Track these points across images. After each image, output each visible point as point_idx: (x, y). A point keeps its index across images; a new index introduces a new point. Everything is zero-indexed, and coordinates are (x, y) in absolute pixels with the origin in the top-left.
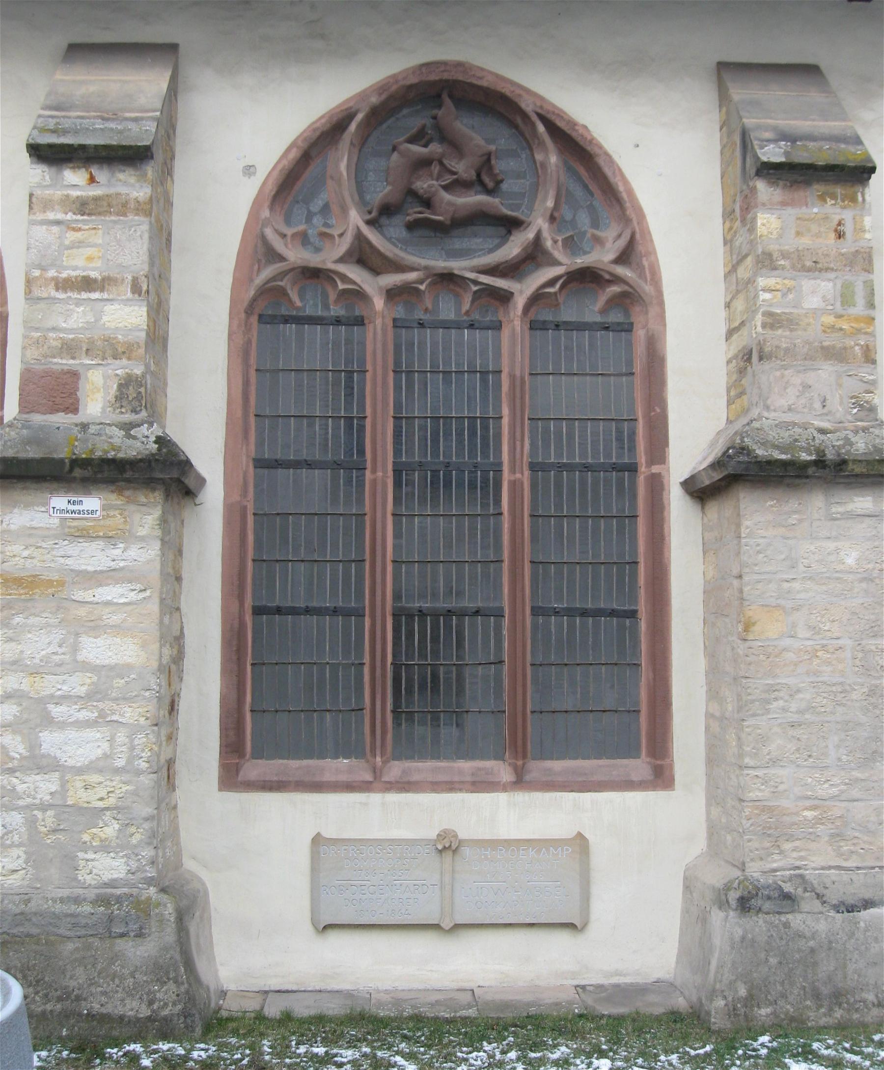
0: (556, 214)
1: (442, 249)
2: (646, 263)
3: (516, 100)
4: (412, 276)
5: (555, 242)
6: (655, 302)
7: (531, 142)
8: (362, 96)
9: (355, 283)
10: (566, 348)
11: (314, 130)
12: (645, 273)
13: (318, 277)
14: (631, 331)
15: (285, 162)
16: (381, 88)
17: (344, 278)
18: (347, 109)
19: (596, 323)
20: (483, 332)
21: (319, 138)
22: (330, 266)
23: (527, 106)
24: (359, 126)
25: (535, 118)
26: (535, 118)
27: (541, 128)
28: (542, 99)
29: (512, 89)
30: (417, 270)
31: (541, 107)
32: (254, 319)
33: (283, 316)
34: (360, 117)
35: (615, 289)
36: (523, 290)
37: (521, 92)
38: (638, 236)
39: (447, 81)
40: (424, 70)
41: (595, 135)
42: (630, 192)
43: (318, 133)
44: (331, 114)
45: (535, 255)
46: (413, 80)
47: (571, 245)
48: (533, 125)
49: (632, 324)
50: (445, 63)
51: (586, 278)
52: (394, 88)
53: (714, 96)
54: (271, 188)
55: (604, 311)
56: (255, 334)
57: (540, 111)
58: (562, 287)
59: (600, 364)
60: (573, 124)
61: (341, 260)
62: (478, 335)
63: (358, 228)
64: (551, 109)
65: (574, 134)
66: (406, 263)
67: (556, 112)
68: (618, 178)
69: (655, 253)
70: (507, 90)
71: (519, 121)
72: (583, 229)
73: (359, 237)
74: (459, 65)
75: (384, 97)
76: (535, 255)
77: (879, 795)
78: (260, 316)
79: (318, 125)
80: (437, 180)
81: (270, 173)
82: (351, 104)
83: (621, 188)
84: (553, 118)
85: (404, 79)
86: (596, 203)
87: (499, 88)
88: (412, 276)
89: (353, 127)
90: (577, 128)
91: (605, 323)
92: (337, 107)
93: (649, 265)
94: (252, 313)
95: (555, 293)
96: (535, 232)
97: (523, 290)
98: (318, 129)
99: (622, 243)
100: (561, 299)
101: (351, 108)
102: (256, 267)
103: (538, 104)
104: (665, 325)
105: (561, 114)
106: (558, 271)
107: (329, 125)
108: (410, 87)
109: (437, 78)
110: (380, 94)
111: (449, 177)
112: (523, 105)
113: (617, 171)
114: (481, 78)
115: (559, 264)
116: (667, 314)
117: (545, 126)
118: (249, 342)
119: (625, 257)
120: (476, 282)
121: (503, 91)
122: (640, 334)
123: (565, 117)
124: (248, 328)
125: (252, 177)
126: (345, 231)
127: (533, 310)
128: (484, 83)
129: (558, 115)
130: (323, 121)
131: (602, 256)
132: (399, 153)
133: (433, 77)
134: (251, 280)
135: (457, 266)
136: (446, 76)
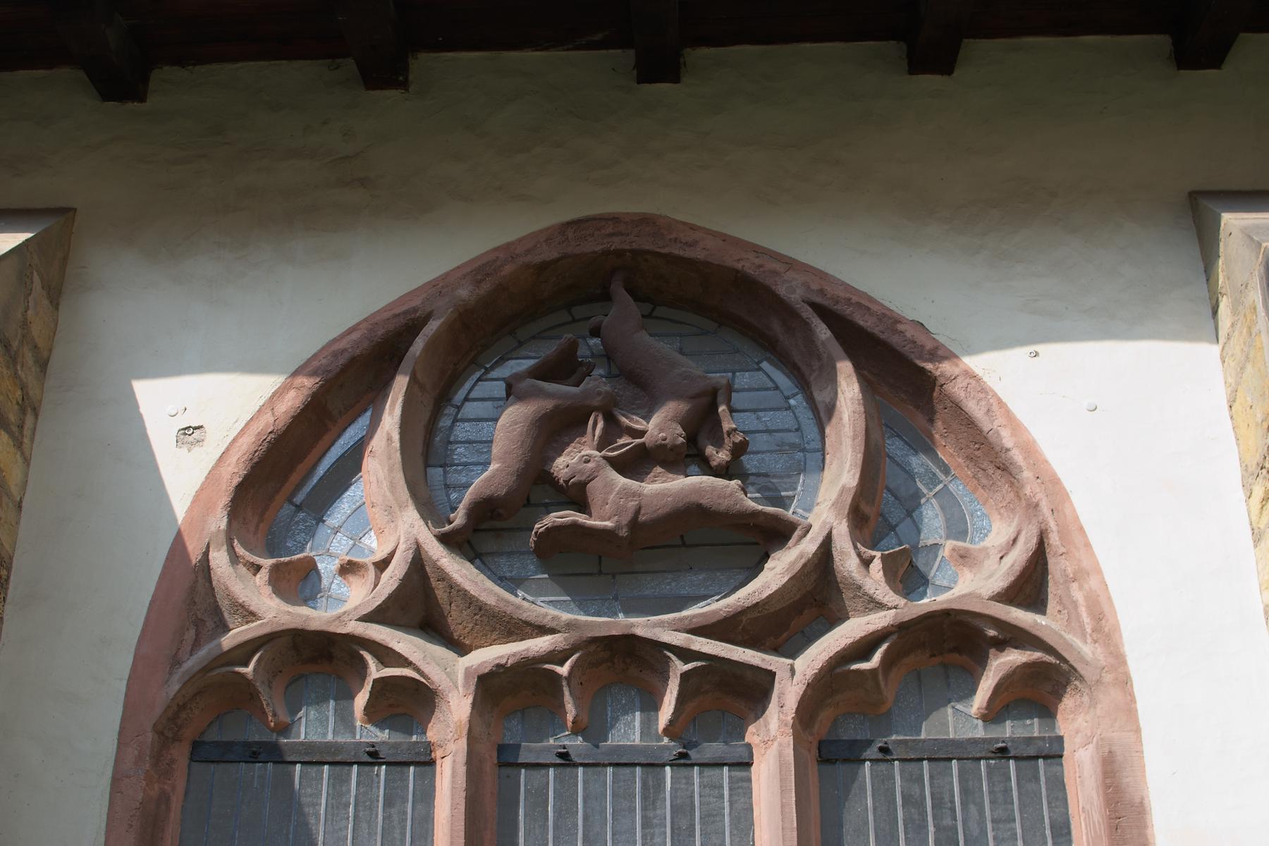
0: (866, 509)
1: (616, 598)
2: (1078, 595)
3: (769, 281)
4: (540, 644)
5: (866, 563)
6: (1108, 678)
7: (804, 368)
8: (439, 287)
9: (406, 663)
10: (907, 800)
11: (335, 355)
12: (1078, 616)
13: (330, 658)
14: (1061, 756)
15: (268, 418)
16: (479, 270)
17: (386, 655)
18: (405, 313)
19: (974, 742)
20: (709, 772)
21: (344, 370)
22: (354, 627)
23: (792, 291)
24: (429, 347)
25: (808, 313)
26: (808, 313)
27: (823, 332)
28: (822, 275)
29: (757, 261)
30: (552, 631)
31: (822, 292)
32: (180, 753)
33: (247, 745)
34: (433, 326)
35: (1014, 658)
36: (793, 675)
37: (778, 267)
38: (1054, 539)
39: (619, 253)
40: (570, 234)
41: (941, 339)
42: (1030, 449)
43: (342, 360)
44: (371, 322)
45: (818, 596)
46: (549, 254)
47: (908, 574)
48: (806, 325)
49: (1060, 739)
50: (615, 219)
51: (950, 643)
52: (508, 269)
53: (1198, 249)
54: (234, 471)
55: (993, 714)
56: (181, 784)
57: (818, 300)
58: (887, 662)
59: (990, 835)
60: (894, 321)
61: (377, 616)
62: (696, 780)
64: (843, 294)
65: (894, 340)
66: (524, 616)
67: (855, 299)
68: (1000, 420)
69: (1099, 571)
70: (748, 264)
71: (777, 327)
72: (930, 542)
73: (418, 563)
74: (645, 220)
75: (486, 286)
76: (818, 596)
77: (709, 815)
78: (196, 745)
79: (342, 344)
80: (600, 449)
81: (234, 440)
82: (416, 302)
83: (1007, 440)
84: (847, 311)
85: (528, 251)
86: (957, 488)
87: (729, 262)
88: (540, 644)
89: (418, 345)
90: (900, 327)
91: (997, 740)
92: (384, 309)
93: (1087, 598)
94: (177, 738)
95: (873, 672)
96: (820, 539)
97: (793, 675)
98: (343, 351)
99: (1019, 556)
100: (889, 693)
101: (415, 310)
102: (190, 635)
103: (815, 287)
104: (1138, 730)
105: (865, 304)
106: (877, 621)
107: (366, 344)
108: (544, 266)
109: (598, 248)
110: (478, 283)
111: (630, 440)
112: (782, 291)
113: (995, 407)
114: (692, 245)
115: (876, 605)
116: (1140, 705)
117: (830, 327)
118: (164, 799)
119: (1031, 585)
120: (686, 654)
121: (739, 266)
122: (1081, 764)
123: (874, 307)
124: (159, 762)
125: (196, 449)
126: (392, 554)
127: (825, 716)
128: (698, 254)
129: (859, 305)
130: (355, 336)
131: (970, 580)
133: (592, 246)
134: (176, 662)
135: (644, 626)
136: (616, 243)
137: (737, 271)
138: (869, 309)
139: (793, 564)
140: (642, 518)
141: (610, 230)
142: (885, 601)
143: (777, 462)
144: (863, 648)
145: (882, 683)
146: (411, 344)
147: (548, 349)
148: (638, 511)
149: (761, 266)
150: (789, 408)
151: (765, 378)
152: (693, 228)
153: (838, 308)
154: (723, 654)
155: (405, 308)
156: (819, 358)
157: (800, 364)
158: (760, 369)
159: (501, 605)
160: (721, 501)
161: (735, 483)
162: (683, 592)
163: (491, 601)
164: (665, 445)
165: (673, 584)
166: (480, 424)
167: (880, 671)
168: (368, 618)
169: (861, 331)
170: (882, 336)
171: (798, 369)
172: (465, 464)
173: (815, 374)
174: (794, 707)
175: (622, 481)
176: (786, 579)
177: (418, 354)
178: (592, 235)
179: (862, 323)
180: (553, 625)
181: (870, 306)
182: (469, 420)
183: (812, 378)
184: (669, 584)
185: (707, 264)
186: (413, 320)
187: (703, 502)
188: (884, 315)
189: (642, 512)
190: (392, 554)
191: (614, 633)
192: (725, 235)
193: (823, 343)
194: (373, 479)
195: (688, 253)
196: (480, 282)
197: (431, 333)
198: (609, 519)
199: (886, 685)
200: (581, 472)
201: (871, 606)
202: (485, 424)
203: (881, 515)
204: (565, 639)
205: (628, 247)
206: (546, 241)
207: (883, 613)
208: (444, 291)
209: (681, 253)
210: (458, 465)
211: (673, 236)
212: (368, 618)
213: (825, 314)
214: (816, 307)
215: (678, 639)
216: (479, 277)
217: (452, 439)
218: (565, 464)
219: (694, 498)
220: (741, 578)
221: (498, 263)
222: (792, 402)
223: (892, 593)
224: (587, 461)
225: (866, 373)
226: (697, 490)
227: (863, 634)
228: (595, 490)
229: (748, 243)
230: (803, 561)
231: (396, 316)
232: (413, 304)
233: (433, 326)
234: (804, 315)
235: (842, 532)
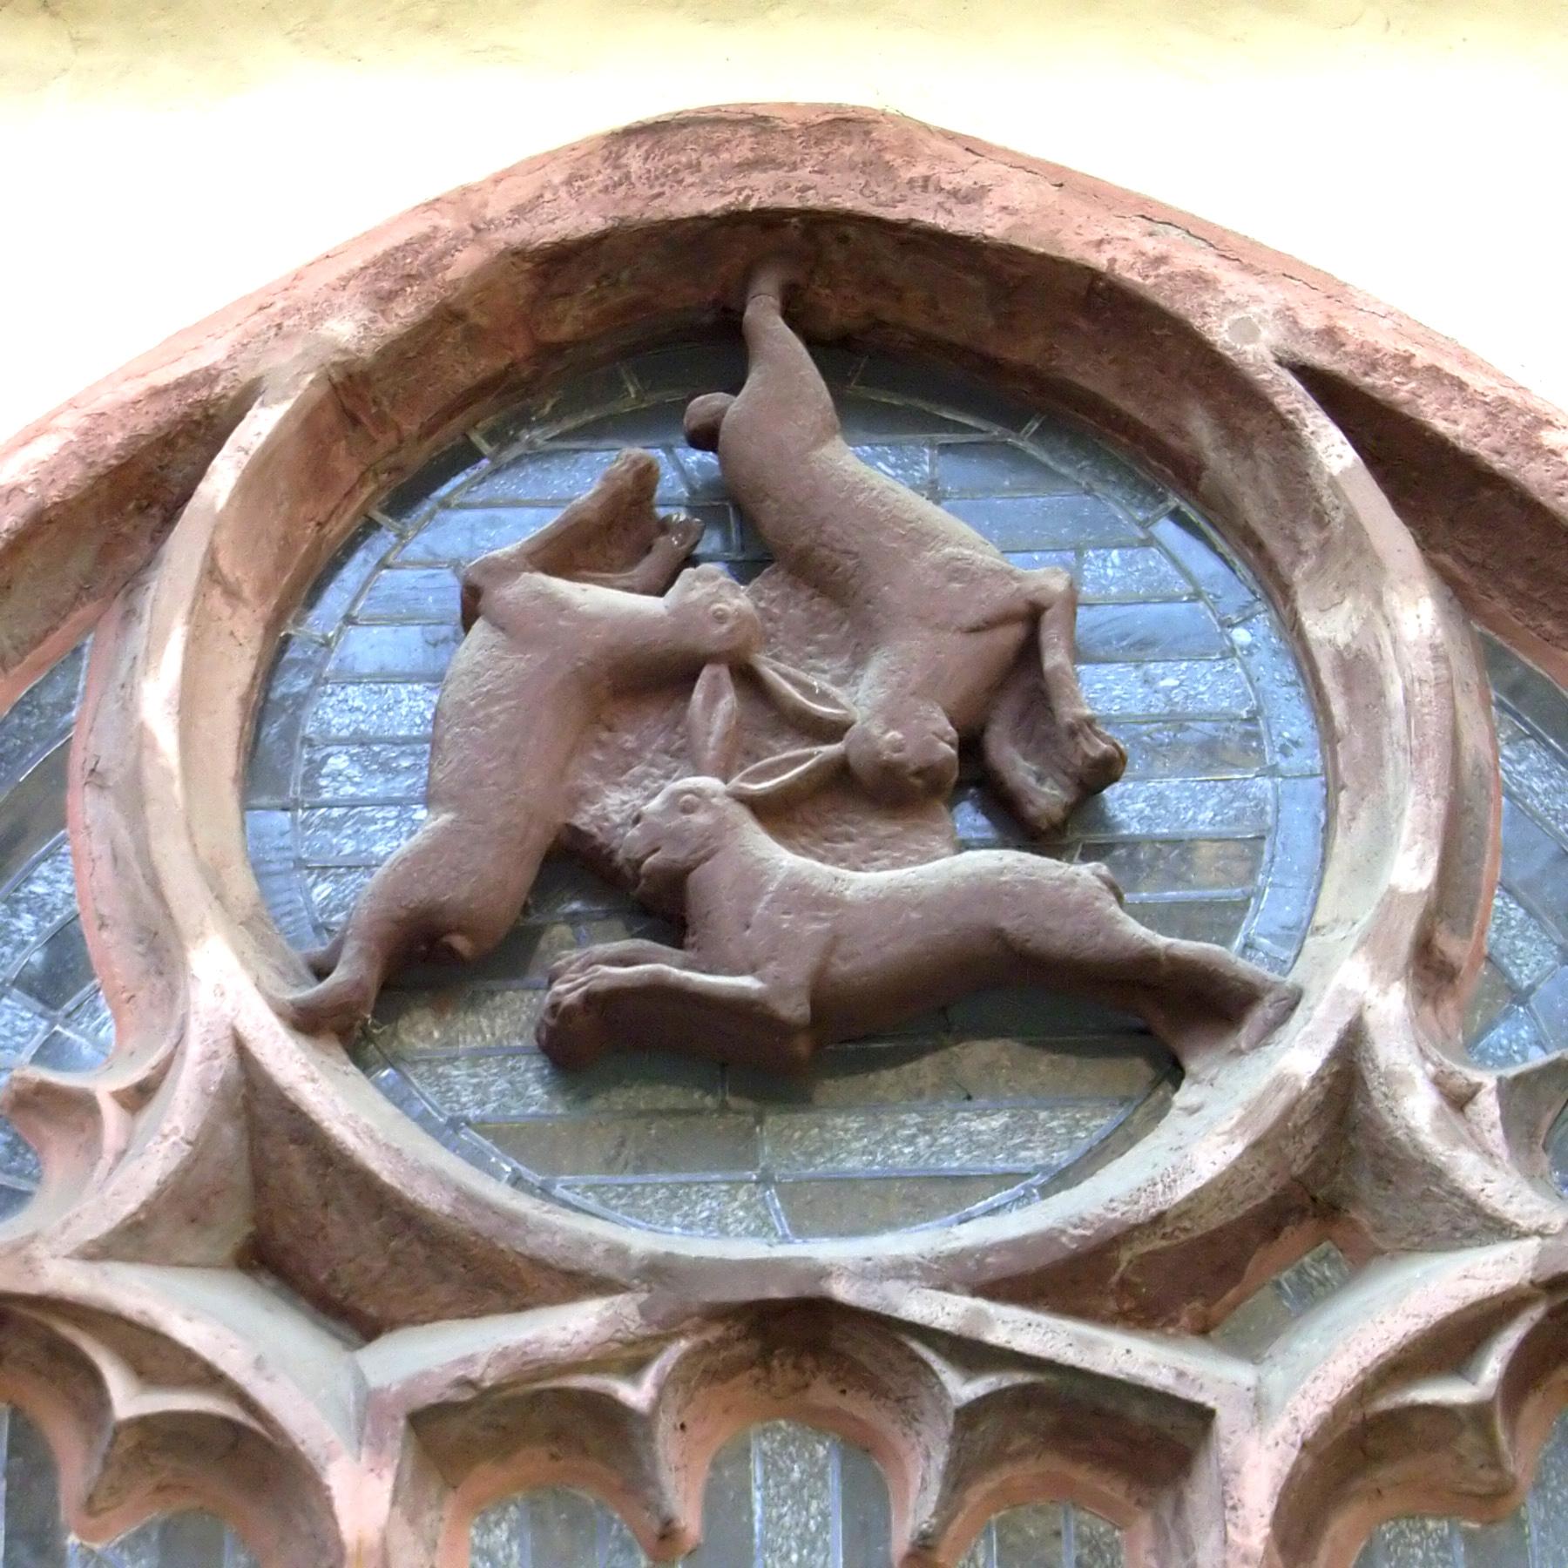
0: (1452, 947)
1: (765, 1180)
3: (1182, 305)
4: (571, 1326)
5: (1458, 1100)
7: (1275, 545)
9: (211, 1378)
17: (153, 1354)
18: (183, 385)
23: (1248, 326)
25: (1292, 397)
26: (1292, 397)
27: (1333, 450)
29: (1151, 247)
31: (1330, 336)
34: (259, 427)
37: (1206, 261)
48: (1286, 432)
52: (466, 261)
57: (1321, 359)
61: (132, 1241)
63: (241, 1048)
66: (531, 1245)
71: (1200, 430)
74: (843, 125)
75: (407, 311)
85: (521, 212)
88: (571, 1326)
89: (222, 479)
95: (1479, 1414)
96: (1329, 1041)
101: (209, 376)
103: (1311, 321)
109: (713, 205)
112: (1220, 333)
114: (972, 196)
120: (970, 1353)
121: (1099, 260)
126: (163, 1070)
132: (499, 626)
135: (849, 1262)
137: (1094, 274)
138: (1461, 386)
139: (1258, 1103)
140: (842, 968)
141: (744, 152)
142: (1510, 1212)
143: (1199, 805)
144: (1452, 1343)
145: (1502, 1437)
146: (199, 474)
147: (580, 480)
148: (832, 944)
149: (1161, 260)
150: (1230, 652)
151: (1167, 568)
152: (973, 147)
153: (1374, 381)
154: (1071, 1356)
155: (181, 370)
156: (1320, 520)
157: (1263, 532)
158: (1149, 542)
159: (468, 1214)
160: (1051, 924)
161: (1087, 873)
162: (950, 1165)
163: (433, 1199)
164: (900, 765)
165: (923, 1141)
166: (390, 691)
167: (1498, 1407)
168: (101, 1251)
169: (1440, 447)
170: (1499, 465)
171: (1259, 547)
172: (353, 803)
173: (1307, 565)
174: (1269, 1509)
175: (783, 860)
176: (1237, 1149)
177: (221, 503)
178: (695, 167)
179: (1441, 426)
180: (610, 1269)
181: (1465, 376)
182: (357, 680)
183: (1298, 575)
184: (911, 1141)
185: (1010, 254)
186: (203, 404)
187: (1008, 924)
188: (1505, 403)
189: (844, 947)
190: (163, 1070)
191: (776, 1292)
192: (1061, 170)
193: (1333, 483)
194: (99, 848)
195: (959, 222)
196: (390, 296)
197: (258, 443)
198: (752, 969)
199: (1513, 1440)
200: (676, 837)
201: (1473, 1223)
202: (403, 691)
203: (1489, 959)
204: (644, 1311)
205: (793, 203)
206: (569, 182)
207: (1504, 1249)
208: (288, 323)
209: (942, 221)
210: (330, 805)
211: (920, 170)
212: (101, 1251)
213: (1333, 393)
214: (1333, 393)
215: (945, 1310)
216: (386, 285)
217: (310, 729)
218: (632, 805)
219: (982, 915)
220: (1102, 1123)
221: (438, 245)
222: (1241, 636)
223: (1528, 1192)
224: (688, 809)
225: (1446, 559)
226: (986, 890)
227: (1451, 1307)
228: (715, 887)
229: (1127, 194)
230: (1283, 1098)
231: (157, 393)
232: (201, 361)
233: (259, 427)
234: (1283, 402)
235: (1390, 1007)
